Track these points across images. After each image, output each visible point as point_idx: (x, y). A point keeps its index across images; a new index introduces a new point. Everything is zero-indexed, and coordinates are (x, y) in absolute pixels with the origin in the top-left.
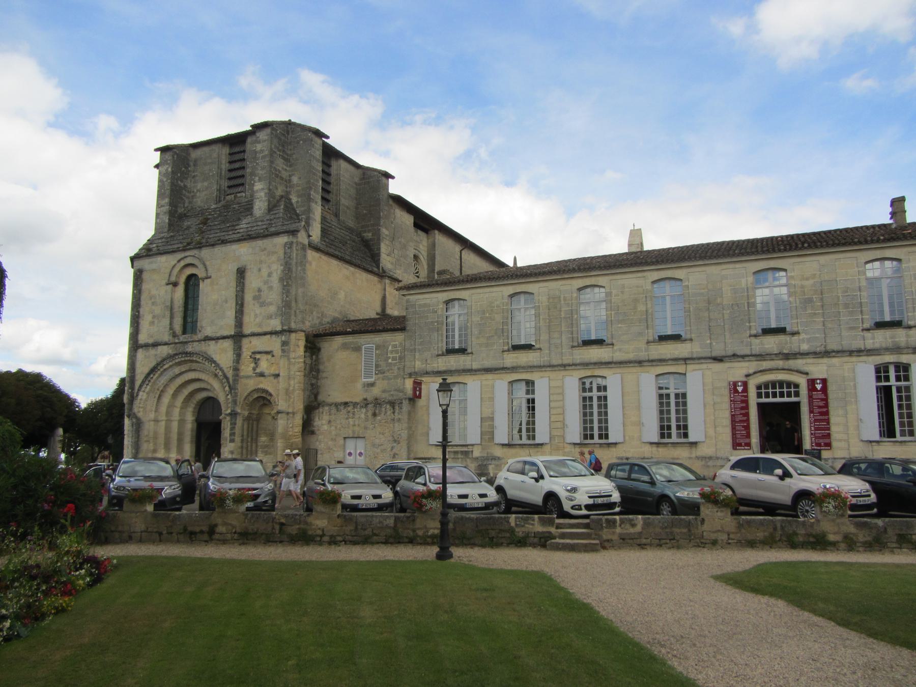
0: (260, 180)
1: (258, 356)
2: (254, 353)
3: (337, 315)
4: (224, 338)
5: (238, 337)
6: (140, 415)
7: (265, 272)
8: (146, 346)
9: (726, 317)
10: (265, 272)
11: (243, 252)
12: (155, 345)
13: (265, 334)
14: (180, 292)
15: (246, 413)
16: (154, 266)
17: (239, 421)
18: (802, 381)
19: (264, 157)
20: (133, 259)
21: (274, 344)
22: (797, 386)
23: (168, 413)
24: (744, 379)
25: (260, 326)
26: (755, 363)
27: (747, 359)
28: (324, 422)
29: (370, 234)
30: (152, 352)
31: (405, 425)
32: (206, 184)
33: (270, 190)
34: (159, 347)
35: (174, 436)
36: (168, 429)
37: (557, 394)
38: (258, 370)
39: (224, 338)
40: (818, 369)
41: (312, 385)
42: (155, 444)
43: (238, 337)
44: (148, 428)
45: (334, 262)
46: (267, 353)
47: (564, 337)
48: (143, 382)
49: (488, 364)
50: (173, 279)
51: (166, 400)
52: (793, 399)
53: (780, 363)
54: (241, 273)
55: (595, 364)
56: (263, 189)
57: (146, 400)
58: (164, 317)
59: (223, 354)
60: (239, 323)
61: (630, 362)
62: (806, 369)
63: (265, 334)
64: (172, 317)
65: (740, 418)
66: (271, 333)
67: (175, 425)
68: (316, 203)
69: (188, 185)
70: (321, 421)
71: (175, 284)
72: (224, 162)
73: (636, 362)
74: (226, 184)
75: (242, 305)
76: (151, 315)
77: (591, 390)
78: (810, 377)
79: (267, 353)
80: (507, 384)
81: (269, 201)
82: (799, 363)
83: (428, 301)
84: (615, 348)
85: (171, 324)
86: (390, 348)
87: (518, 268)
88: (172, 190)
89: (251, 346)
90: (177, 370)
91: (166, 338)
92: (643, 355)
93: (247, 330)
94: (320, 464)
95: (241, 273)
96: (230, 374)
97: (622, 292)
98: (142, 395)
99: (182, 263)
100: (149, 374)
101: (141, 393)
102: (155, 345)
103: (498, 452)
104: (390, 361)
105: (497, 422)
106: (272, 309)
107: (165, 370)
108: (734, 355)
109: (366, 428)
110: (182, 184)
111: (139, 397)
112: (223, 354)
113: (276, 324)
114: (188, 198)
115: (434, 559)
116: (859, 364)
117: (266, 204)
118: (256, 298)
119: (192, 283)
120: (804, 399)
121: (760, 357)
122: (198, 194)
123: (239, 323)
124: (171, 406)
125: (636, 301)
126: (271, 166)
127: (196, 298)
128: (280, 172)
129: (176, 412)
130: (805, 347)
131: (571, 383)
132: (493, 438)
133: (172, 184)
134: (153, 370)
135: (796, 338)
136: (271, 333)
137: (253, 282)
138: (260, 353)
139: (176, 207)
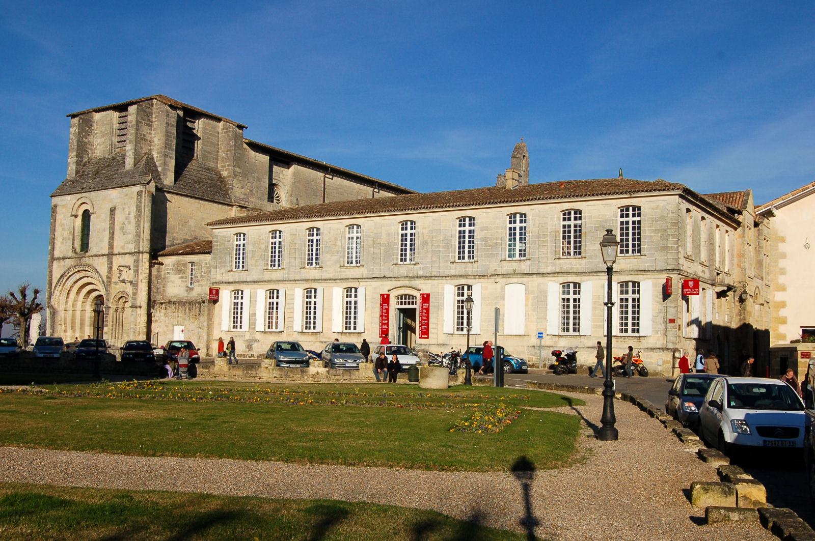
0: (130, 143)
1: (122, 269)
2: (119, 267)
3: (187, 237)
4: (103, 255)
5: (110, 255)
6: (56, 306)
7: (127, 210)
8: (58, 259)
9: (382, 251)
10: (127, 210)
11: (114, 196)
12: (64, 258)
13: (126, 254)
14: (79, 222)
16: (64, 203)
18: (417, 294)
19: (132, 126)
21: (129, 260)
22: (413, 297)
23: (74, 305)
24: (388, 293)
25: (123, 247)
28: (162, 314)
29: (226, 173)
30: (62, 263)
31: (206, 317)
32: (103, 140)
33: (135, 150)
34: (67, 260)
35: (78, 321)
36: (73, 316)
37: (290, 300)
38: (121, 279)
39: (103, 255)
40: (426, 287)
42: (66, 327)
43: (110, 255)
44: (61, 315)
46: (127, 267)
47: (297, 261)
48: (57, 284)
49: (255, 278)
50: (74, 213)
52: (411, 306)
53: (407, 283)
54: (113, 211)
55: (311, 280)
56: (131, 149)
57: (60, 296)
58: (69, 239)
59: (101, 265)
60: (111, 246)
61: (330, 279)
62: (419, 287)
63: (126, 254)
64: (74, 240)
66: (130, 253)
67: (78, 314)
68: (170, 157)
69: (92, 140)
70: (158, 314)
71: (76, 216)
72: (115, 123)
73: (333, 280)
74: (127, 136)
75: (113, 233)
76: (62, 238)
78: (421, 292)
79: (127, 267)
80: (302, 290)
81: (135, 158)
83: (225, 234)
86: (203, 265)
87: (327, 205)
88: (78, 146)
89: (117, 261)
90: (78, 276)
91: (70, 254)
92: (337, 276)
93: (116, 251)
95: (113, 211)
96: (105, 280)
97: (330, 233)
98: (57, 293)
99: (80, 201)
100: (60, 278)
101: (56, 292)
102: (64, 258)
103: (258, 336)
104: (203, 274)
105: (257, 317)
106: (130, 237)
107: (70, 276)
109: (185, 319)
110: (86, 140)
111: (55, 294)
112: (101, 265)
113: (131, 248)
114: (91, 150)
116: (550, 282)
117: (133, 160)
118: (122, 229)
119: (86, 215)
120: (417, 307)
122: (98, 147)
123: (111, 246)
124: (75, 301)
125: (336, 239)
126: (137, 133)
127: (88, 226)
128: (144, 135)
129: (79, 304)
130: (421, 273)
131: (261, 294)
132: (255, 327)
133: (78, 141)
134: (62, 276)
135: (416, 266)
136: (130, 253)
137: (119, 217)
138: (123, 267)
139: (82, 157)
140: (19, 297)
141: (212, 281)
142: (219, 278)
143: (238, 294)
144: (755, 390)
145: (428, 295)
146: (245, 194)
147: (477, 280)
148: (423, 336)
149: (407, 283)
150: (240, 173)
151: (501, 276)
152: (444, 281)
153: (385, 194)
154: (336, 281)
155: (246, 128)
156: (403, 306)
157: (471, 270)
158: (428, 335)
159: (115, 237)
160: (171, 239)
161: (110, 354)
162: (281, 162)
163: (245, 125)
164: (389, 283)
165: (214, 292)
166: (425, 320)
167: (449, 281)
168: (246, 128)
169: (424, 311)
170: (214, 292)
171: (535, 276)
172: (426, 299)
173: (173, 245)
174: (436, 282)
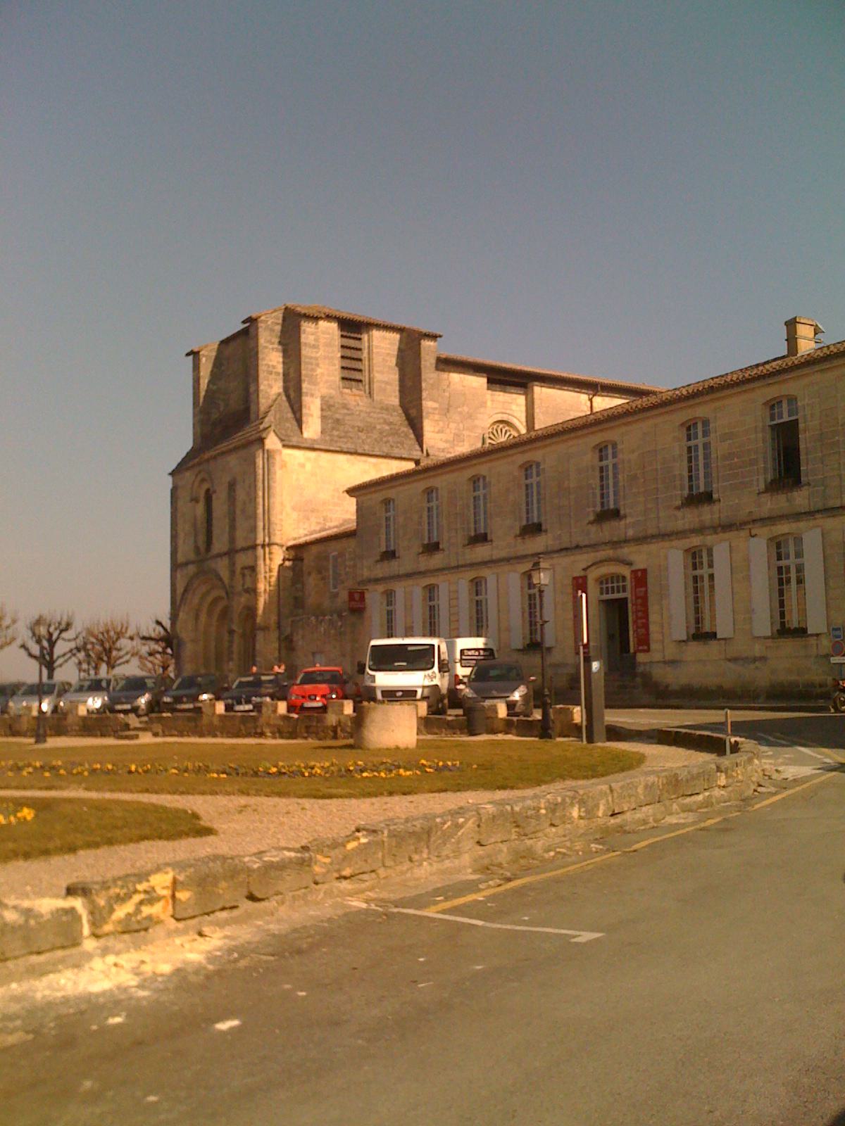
15: (241, 631)
17: (236, 638)
18: (626, 571)
20: (172, 474)
22: (624, 578)
24: (582, 574)
26: (593, 554)
27: (584, 550)
40: (640, 557)
41: (296, 598)
45: (342, 458)
51: (203, 617)
52: (621, 595)
53: (609, 553)
60: (232, 539)
64: (196, 536)
65: (640, 614)
77: (788, 557)
78: (634, 568)
82: (625, 551)
84: (494, 544)
85: (196, 542)
86: (347, 556)
94: (547, 646)
104: (347, 569)
108: (577, 547)
115: (606, 723)
118: (243, 511)
121: (593, 546)
123: (232, 539)
140: (159, 629)
141: (359, 579)
142: (366, 573)
143: (389, 595)
144: (410, 648)
145: (644, 571)
146: (446, 441)
147: (722, 535)
148: (641, 648)
149: (609, 553)
150: (435, 409)
151: (759, 524)
152: (667, 544)
153: (603, 403)
154: (511, 561)
155: (440, 336)
156: (610, 596)
157: (709, 517)
158: (648, 645)
159: (238, 524)
160: (321, 521)
161: (144, 695)
162: (510, 385)
163: (438, 333)
164: (585, 556)
165: (357, 596)
166: (641, 618)
167: (675, 543)
168: (440, 336)
169: (639, 601)
170: (357, 596)
171: (818, 516)
172: (641, 578)
173: (326, 530)
174: (653, 547)
